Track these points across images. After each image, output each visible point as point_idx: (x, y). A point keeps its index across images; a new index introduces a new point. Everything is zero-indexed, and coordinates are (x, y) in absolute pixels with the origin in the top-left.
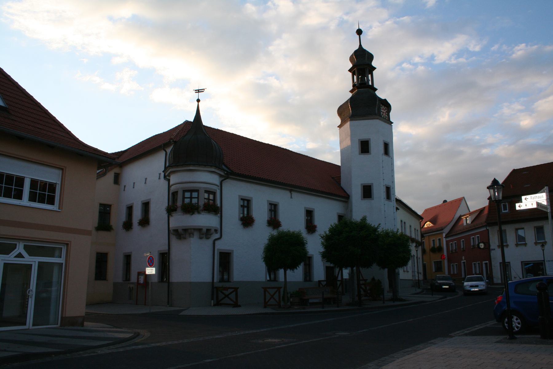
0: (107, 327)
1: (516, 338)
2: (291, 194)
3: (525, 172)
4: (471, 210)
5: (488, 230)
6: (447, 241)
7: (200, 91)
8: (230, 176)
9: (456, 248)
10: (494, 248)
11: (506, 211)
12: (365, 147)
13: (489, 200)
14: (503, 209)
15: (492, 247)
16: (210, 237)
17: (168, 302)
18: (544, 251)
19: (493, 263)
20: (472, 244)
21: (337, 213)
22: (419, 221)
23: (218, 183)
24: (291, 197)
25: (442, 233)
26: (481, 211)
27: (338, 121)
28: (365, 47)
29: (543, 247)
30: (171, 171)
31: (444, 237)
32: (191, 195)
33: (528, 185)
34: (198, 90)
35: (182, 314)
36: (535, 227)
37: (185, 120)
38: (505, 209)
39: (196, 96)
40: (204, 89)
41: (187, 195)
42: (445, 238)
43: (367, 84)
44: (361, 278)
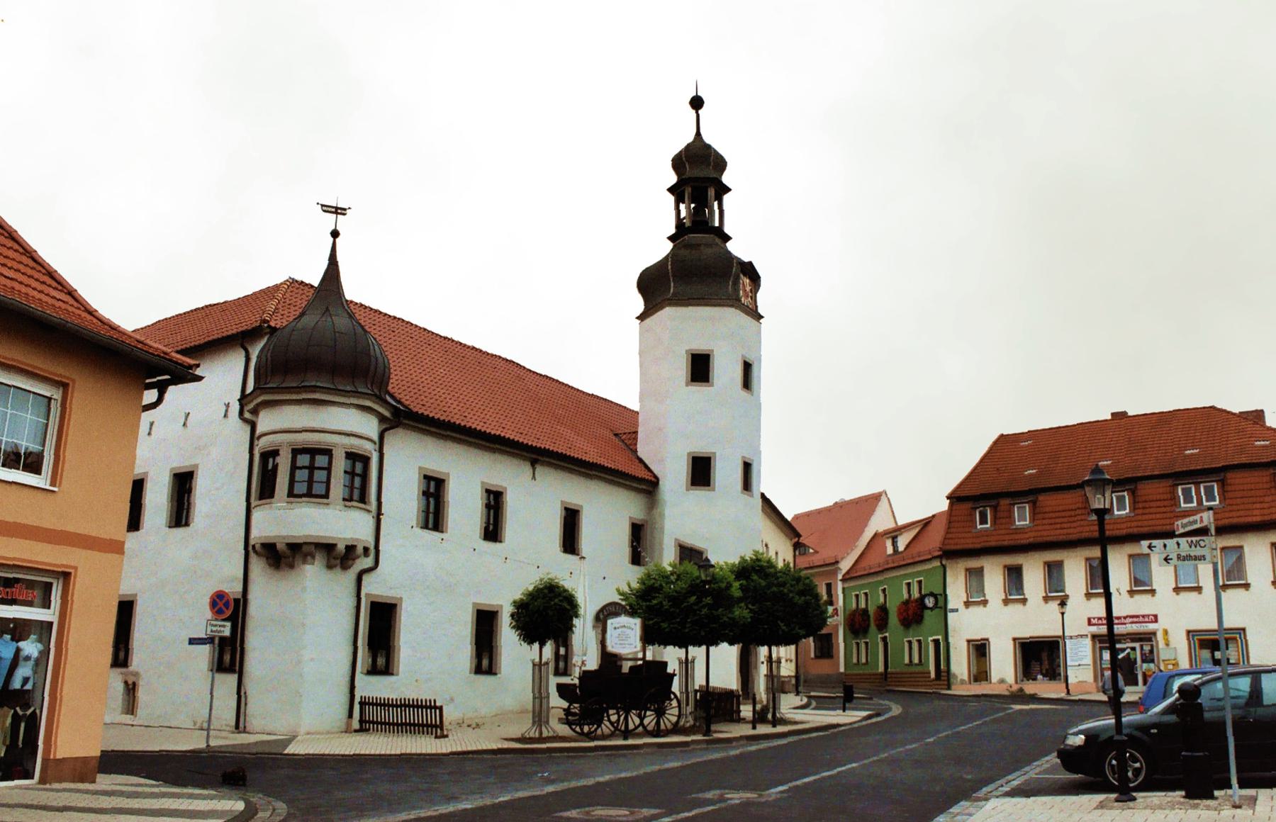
0: (146, 785)
1: (1134, 799)
4: (901, 522)
7: (333, 210)
11: (1024, 523)
12: (700, 368)
13: (948, 501)
14: (978, 523)
15: (950, 606)
16: (353, 564)
17: (237, 726)
18: (1065, 615)
22: (791, 540)
23: (375, 437)
24: (534, 477)
26: (926, 523)
27: (639, 304)
28: (708, 138)
29: (1062, 607)
30: (262, 401)
32: (312, 460)
35: (290, 750)
36: (1045, 563)
37: (287, 278)
38: (983, 521)
40: (345, 209)
41: (304, 460)
43: (710, 225)
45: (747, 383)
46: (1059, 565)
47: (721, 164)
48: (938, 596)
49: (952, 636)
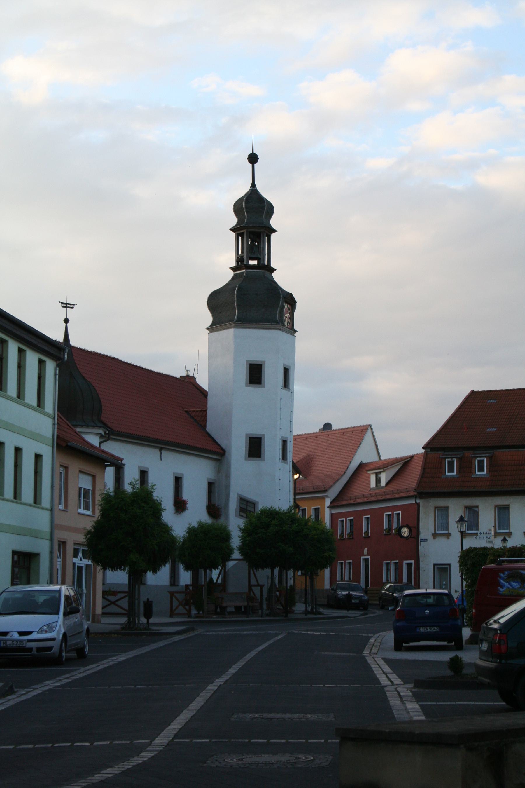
2: (161, 454)
3: (491, 400)
4: (384, 457)
5: (418, 505)
6: (332, 515)
7: (68, 306)
8: (112, 437)
9: (351, 531)
10: (426, 538)
15: (422, 536)
19: (421, 564)
20: (385, 526)
21: (207, 479)
24: (161, 459)
25: (324, 498)
27: (208, 318)
31: (328, 507)
33: (493, 430)
34: (66, 304)
36: (496, 506)
39: (62, 313)
40: (74, 305)
42: (328, 509)
44: (253, 582)
45: (286, 384)
46: (506, 508)
47: (269, 209)
48: (412, 528)
49: (422, 561)
